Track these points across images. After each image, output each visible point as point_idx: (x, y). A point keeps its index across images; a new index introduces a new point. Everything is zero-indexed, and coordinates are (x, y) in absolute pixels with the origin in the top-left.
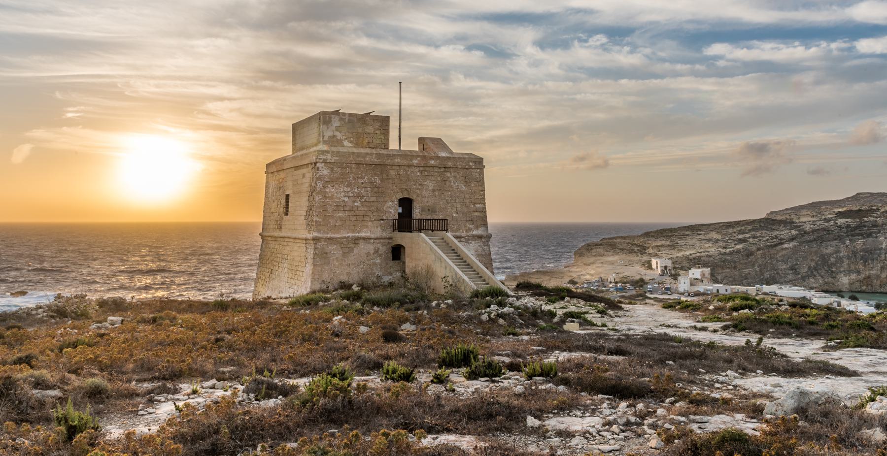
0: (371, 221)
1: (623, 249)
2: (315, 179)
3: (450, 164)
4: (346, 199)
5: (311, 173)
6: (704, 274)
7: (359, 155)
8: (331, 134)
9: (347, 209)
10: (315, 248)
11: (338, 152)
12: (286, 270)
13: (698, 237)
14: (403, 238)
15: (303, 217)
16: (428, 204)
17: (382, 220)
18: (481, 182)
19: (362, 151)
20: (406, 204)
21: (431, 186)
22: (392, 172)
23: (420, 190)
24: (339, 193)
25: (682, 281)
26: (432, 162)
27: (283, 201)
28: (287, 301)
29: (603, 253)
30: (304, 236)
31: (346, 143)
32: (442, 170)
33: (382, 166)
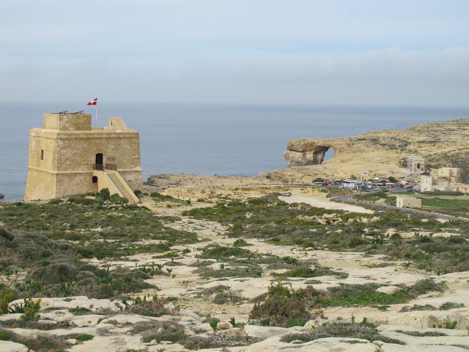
1: (384, 145)
2: (56, 147)
3: (121, 136)
6: (453, 173)
7: (76, 134)
8: (63, 125)
10: (57, 178)
11: (67, 134)
12: (43, 187)
13: (463, 133)
14: (97, 173)
15: (51, 163)
16: (111, 156)
17: (88, 164)
20: (99, 157)
21: (112, 147)
24: (68, 153)
25: (425, 181)
26: (113, 136)
27: (40, 153)
28: (47, 202)
29: (363, 148)
30: (52, 172)
31: (70, 129)
32: (118, 139)
33: (88, 139)
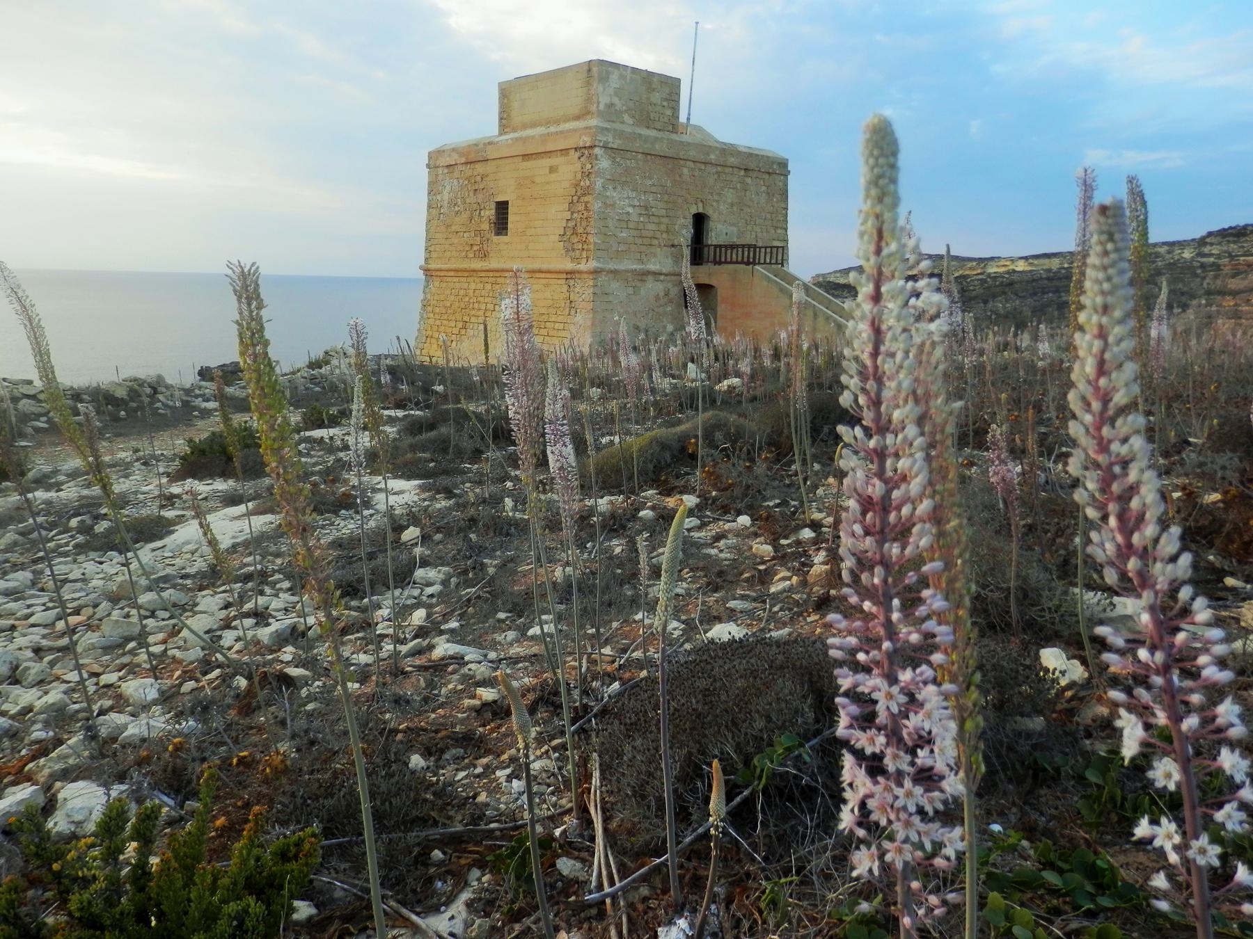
0: (660, 246)
4: (630, 210)
5: (579, 165)
9: (631, 225)
18: (784, 194)
19: (652, 133)
22: (685, 171)
23: (717, 201)
